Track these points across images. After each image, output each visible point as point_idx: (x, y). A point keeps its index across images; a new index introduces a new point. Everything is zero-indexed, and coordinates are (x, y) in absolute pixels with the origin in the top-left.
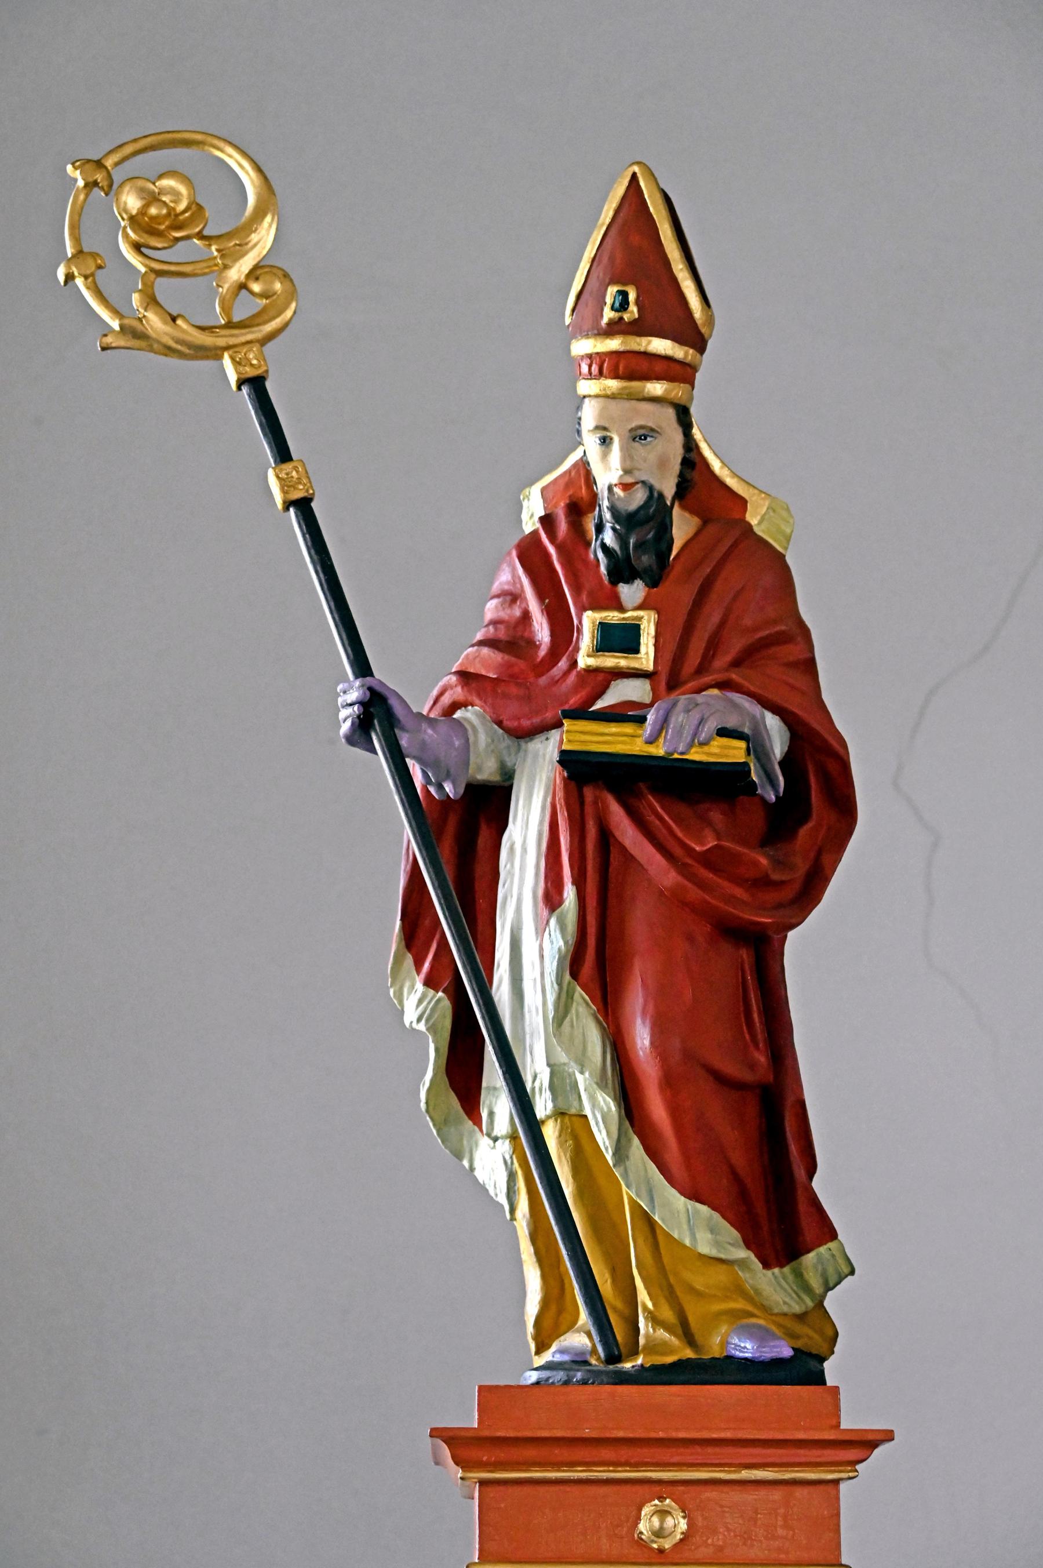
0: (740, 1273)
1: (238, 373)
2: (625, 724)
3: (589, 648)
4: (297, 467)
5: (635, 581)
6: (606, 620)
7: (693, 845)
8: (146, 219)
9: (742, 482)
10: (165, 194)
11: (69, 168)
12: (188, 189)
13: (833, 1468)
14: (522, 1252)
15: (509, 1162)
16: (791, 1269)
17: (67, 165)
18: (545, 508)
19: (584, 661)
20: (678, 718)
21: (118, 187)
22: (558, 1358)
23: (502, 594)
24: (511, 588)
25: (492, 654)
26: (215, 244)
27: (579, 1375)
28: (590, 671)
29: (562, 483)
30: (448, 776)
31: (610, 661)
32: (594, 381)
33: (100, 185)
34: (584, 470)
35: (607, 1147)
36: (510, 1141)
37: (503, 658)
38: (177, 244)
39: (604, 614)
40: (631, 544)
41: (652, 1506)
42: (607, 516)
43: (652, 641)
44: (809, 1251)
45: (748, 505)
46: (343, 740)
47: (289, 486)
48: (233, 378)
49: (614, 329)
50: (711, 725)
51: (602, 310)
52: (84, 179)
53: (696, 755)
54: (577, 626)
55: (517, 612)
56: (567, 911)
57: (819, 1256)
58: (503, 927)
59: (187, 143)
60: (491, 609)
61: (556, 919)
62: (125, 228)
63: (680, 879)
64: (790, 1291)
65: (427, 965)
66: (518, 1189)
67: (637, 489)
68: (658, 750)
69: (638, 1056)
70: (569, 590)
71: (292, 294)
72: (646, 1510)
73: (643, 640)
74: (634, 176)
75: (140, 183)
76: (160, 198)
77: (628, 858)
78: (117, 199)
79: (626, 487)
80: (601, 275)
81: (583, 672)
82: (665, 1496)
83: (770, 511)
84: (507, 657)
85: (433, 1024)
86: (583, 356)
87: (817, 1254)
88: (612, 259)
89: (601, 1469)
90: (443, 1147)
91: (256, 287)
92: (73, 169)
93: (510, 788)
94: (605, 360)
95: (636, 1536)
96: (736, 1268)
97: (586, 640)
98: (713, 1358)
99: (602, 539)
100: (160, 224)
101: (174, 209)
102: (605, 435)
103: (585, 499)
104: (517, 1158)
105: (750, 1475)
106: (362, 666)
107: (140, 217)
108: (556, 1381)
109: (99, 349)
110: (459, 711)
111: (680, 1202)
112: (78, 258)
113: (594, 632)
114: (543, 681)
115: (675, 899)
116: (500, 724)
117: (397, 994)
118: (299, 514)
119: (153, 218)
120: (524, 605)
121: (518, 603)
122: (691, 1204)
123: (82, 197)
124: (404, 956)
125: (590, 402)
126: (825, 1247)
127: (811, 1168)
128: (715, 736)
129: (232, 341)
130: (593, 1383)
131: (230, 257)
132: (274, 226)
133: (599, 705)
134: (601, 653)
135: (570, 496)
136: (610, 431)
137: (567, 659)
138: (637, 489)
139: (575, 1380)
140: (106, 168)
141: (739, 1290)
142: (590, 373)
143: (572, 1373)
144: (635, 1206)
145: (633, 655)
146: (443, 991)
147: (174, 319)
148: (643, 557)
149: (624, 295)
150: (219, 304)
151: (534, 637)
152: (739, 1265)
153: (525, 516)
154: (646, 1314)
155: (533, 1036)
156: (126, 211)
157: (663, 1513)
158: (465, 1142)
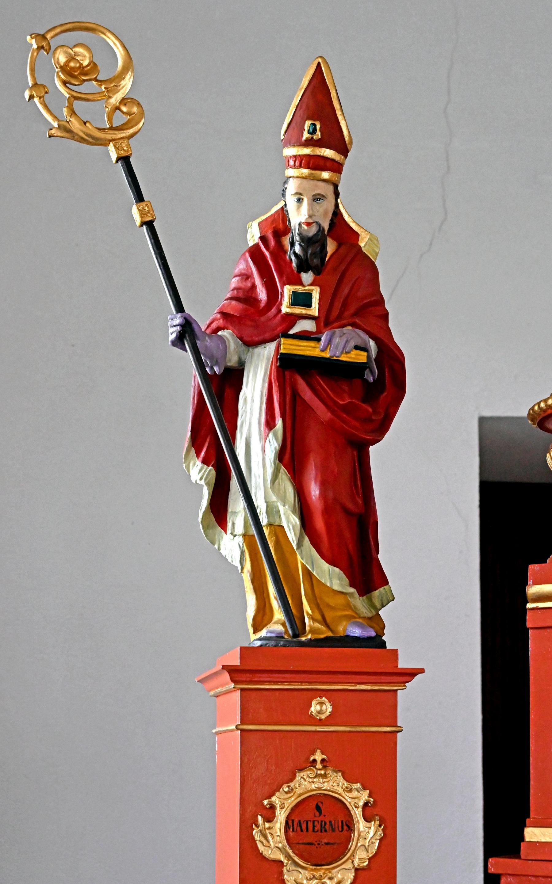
0: (349, 598)
1: (118, 154)
2: (311, 342)
3: (287, 304)
4: (148, 205)
5: (309, 272)
6: (296, 290)
7: (339, 401)
8: (68, 68)
9: (357, 225)
10: (78, 56)
11: (28, 38)
12: (89, 54)
13: (396, 685)
14: (245, 587)
15: (241, 546)
16: (366, 597)
17: (27, 36)
18: (260, 233)
19: (285, 309)
20: (336, 340)
21: (54, 50)
22: (269, 635)
23: (240, 275)
24: (246, 272)
25: (237, 304)
26: (104, 84)
27: (282, 643)
28: (287, 315)
29: (270, 220)
30: (217, 363)
31: (298, 310)
32: (297, 169)
33: (45, 48)
34: (283, 213)
35: (294, 540)
36: (242, 537)
37: (242, 307)
38: (84, 83)
39: (295, 287)
40: (309, 253)
41: (317, 700)
42: (297, 238)
43: (317, 302)
44: (376, 590)
45: (360, 236)
46: (170, 343)
47: (144, 214)
48: (114, 156)
49: (309, 143)
50: (352, 344)
51: (303, 133)
52: (37, 45)
53: (344, 358)
54: (281, 292)
55: (249, 284)
56: (278, 431)
57: (380, 592)
58: (241, 437)
59: (87, 29)
60: (234, 282)
61: (272, 434)
62: (58, 73)
63: (332, 417)
64: (367, 608)
65: (203, 454)
66: (245, 559)
67: (313, 226)
68: (327, 355)
69: (311, 499)
70: (277, 275)
71: (142, 114)
72: (314, 703)
73: (313, 301)
74: (319, 63)
75: (65, 49)
76: (75, 58)
77: (307, 407)
78: (54, 57)
79: (308, 224)
80: (302, 115)
81: (284, 315)
82: (322, 696)
83: (369, 240)
84: (245, 306)
85: (208, 481)
86: (291, 156)
87: (379, 591)
88: (308, 107)
89: (314, 684)
90: (206, 539)
91: (124, 109)
92: (31, 38)
93: (242, 371)
94: (303, 159)
95: (309, 713)
96: (348, 597)
97: (286, 300)
98: (341, 636)
99: (294, 250)
100: (75, 72)
101: (82, 64)
102: (300, 197)
103: (281, 229)
104: (245, 544)
105: (360, 687)
106: (180, 308)
107: (65, 67)
108: (270, 645)
109: (48, 136)
110: (220, 331)
111: (326, 566)
112: (36, 87)
113: (290, 296)
114: (263, 319)
115: (329, 426)
116: (241, 339)
117: (187, 467)
118: (148, 229)
119: (72, 68)
120: (252, 281)
121: (250, 279)
122: (331, 567)
123: (35, 54)
124: (191, 449)
125: (293, 180)
126: (383, 588)
127: (378, 551)
128: (353, 349)
129: (114, 137)
130: (288, 646)
131: (111, 91)
132: (132, 77)
133: (292, 332)
134: (293, 306)
135: (274, 228)
136: (302, 195)
137: (276, 309)
138: (313, 226)
139: (280, 645)
140: (46, 39)
141: (349, 606)
142: (295, 165)
143: (278, 642)
144: (304, 568)
145: (308, 308)
146: (212, 466)
147: (85, 123)
148: (314, 260)
149: (315, 125)
150: (107, 117)
151: (257, 297)
152: (349, 596)
153: (249, 236)
154: (309, 616)
155: (256, 488)
156: (59, 64)
157: (321, 704)
158: (216, 537)
